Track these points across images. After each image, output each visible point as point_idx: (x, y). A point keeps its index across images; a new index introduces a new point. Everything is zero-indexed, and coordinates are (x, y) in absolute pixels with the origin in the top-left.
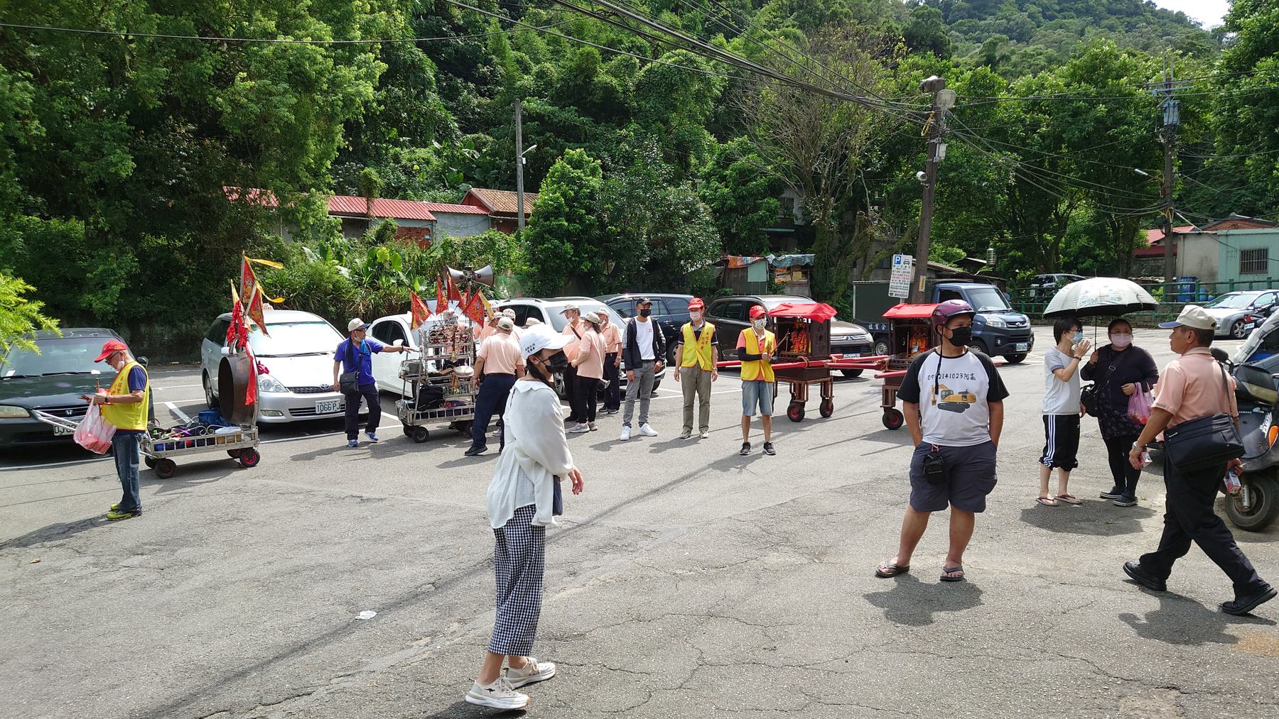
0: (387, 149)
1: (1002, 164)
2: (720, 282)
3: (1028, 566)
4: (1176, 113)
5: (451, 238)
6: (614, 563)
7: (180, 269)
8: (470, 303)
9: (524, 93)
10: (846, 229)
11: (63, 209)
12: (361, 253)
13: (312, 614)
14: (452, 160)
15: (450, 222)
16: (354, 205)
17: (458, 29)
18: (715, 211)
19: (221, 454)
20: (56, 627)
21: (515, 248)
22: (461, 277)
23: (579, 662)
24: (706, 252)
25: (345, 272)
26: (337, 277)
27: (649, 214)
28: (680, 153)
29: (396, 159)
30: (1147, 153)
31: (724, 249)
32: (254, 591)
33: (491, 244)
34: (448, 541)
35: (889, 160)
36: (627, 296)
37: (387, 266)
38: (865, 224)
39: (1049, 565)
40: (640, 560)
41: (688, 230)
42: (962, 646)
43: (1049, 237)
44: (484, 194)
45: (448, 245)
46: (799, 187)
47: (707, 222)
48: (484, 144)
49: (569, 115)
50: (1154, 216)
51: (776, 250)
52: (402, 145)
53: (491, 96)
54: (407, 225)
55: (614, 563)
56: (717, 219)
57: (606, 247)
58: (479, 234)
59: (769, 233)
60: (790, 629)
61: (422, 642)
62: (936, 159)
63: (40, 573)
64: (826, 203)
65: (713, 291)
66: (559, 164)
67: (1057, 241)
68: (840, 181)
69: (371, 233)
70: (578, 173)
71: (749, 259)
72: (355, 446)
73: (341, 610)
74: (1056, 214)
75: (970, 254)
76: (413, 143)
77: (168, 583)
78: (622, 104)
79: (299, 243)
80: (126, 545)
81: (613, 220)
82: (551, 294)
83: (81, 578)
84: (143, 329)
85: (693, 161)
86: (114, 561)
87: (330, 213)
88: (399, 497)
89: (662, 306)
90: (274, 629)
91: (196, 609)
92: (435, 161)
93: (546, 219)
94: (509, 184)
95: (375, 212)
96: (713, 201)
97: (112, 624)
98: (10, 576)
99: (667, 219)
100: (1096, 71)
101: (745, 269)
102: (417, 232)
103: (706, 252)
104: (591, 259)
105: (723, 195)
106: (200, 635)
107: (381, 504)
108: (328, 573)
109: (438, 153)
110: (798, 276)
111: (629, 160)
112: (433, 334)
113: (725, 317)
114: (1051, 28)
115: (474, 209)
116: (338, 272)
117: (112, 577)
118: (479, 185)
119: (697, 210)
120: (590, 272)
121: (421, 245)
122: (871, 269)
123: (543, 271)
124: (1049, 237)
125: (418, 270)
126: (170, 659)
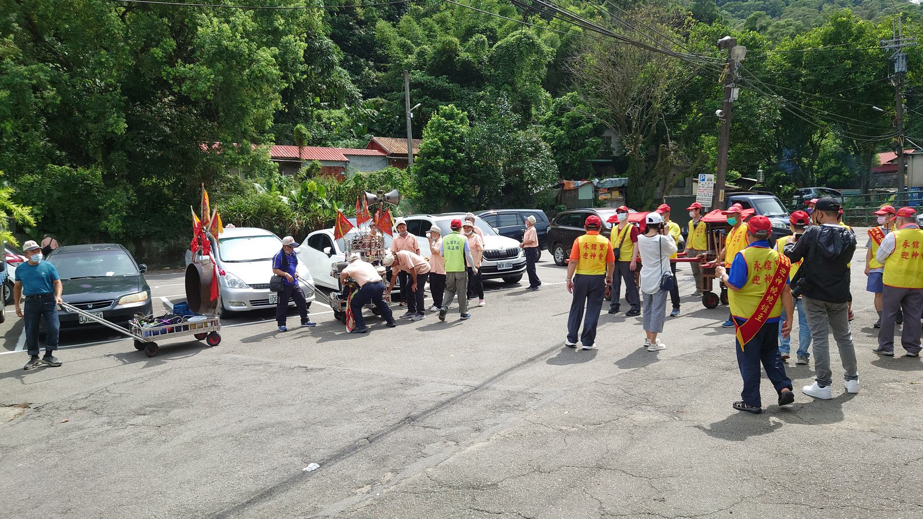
0: (312, 112)
1: (768, 105)
2: (558, 200)
3: (859, 422)
4: (905, 63)
5: (360, 173)
6: (510, 420)
7: (169, 201)
8: (381, 220)
9: (409, 67)
10: (651, 158)
11: (80, 157)
13: (275, 465)
14: (360, 118)
15: (359, 162)
17: (361, 23)
18: (553, 148)
19: (189, 337)
20: (78, 476)
21: (407, 178)
22: (375, 199)
23: (497, 510)
24: (547, 178)
25: (285, 199)
26: (280, 204)
27: (504, 151)
28: (524, 106)
29: (319, 118)
30: (879, 92)
31: (560, 176)
32: (230, 444)
33: (389, 177)
34: (376, 403)
35: (683, 105)
36: (492, 212)
37: (315, 194)
38: (666, 154)
39: (877, 421)
40: (529, 417)
41: (533, 163)
42: (827, 497)
43: (805, 161)
44: (383, 141)
45: (358, 178)
46: (616, 128)
47: (548, 156)
49: (442, 82)
50: (883, 142)
51: (600, 176)
52: (322, 108)
53: (385, 70)
54: (329, 165)
55: (510, 420)
56: (555, 154)
57: (473, 177)
58: (379, 170)
59: (594, 163)
60: (672, 481)
61: (365, 490)
62: (731, 100)
63: (68, 431)
64: (637, 139)
65: (553, 207)
66: (434, 118)
67: (811, 164)
68: (647, 123)
69: (303, 171)
70: (451, 122)
71: (580, 183)
72: (286, 330)
73: (297, 461)
74: (811, 143)
75: (744, 175)
76: (330, 106)
77: (164, 438)
78: (478, 71)
79: (250, 180)
80: (133, 407)
81: (478, 156)
82: (437, 211)
83: (98, 434)
84: (144, 244)
85: (534, 112)
86: (123, 421)
87: (273, 158)
88: (335, 367)
89: (519, 219)
90: (248, 476)
91: (185, 460)
93: (429, 158)
94: (400, 133)
96: (552, 140)
97: (121, 473)
98: (45, 433)
99: (518, 155)
100: (841, 33)
101: (576, 190)
102: (336, 169)
103: (547, 178)
104: (462, 186)
105: (560, 136)
107: (321, 373)
108: (286, 430)
109: (348, 113)
110: (616, 194)
111: (488, 112)
112: (355, 242)
113: (568, 225)
114: (797, 6)
115: (375, 152)
117: (122, 433)
118: (378, 134)
119: (540, 147)
120: (462, 195)
121: (338, 179)
122: (670, 189)
123: (428, 195)
124: (805, 161)
126: (166, 504)
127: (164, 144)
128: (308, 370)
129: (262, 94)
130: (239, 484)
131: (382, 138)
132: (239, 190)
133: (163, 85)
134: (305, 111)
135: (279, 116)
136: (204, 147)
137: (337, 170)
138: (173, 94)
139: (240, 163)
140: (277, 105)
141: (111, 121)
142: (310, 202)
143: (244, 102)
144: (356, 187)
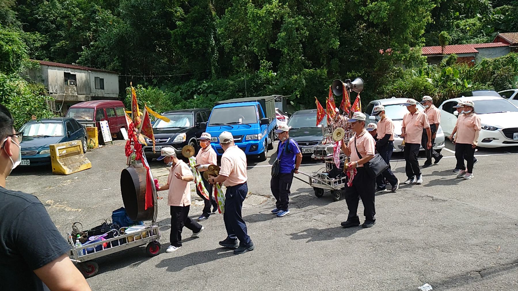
0: (453, 22)
11: (317, 64)
12: (438, 71)
13: (397, 276)
15: (486, 52)
16: (436, 50)
25: (430, 80)
26: (426, 83)
29: (458, 26)
32: (368, 249)
34: (489, 239)
37: (451, 76)
45: (486, 62)
48: (507, 11)
69: (444, 61)
73: (415, 277)
76: (467, 17)
83: (296, 222)
87: (422, 55)
88: (455, 200)
92: (478, 24)
95: (446, 52)
106: (336, 272)
107: (444, 204)
108: (409, 247)
109: (479, 19)
115: (500, 44)
116: (427, 81)
121: (469, 65)
125: (468, 77)
127: (360, 51)
128: (433, 200)
129: (418, 13)
130: (368, 285)
131: (506, 34)
132: (399, 75)
133: (360, 17)
134: (447, 22)
135: (430, 27)
136: (381, 51)
137: (468, 59)
138: (365, 22)
139: (403, 59)
140: (428, 20)
141: (332, 42)
142: (447, 81)
143: (406, 20)
144: (483, 69)
